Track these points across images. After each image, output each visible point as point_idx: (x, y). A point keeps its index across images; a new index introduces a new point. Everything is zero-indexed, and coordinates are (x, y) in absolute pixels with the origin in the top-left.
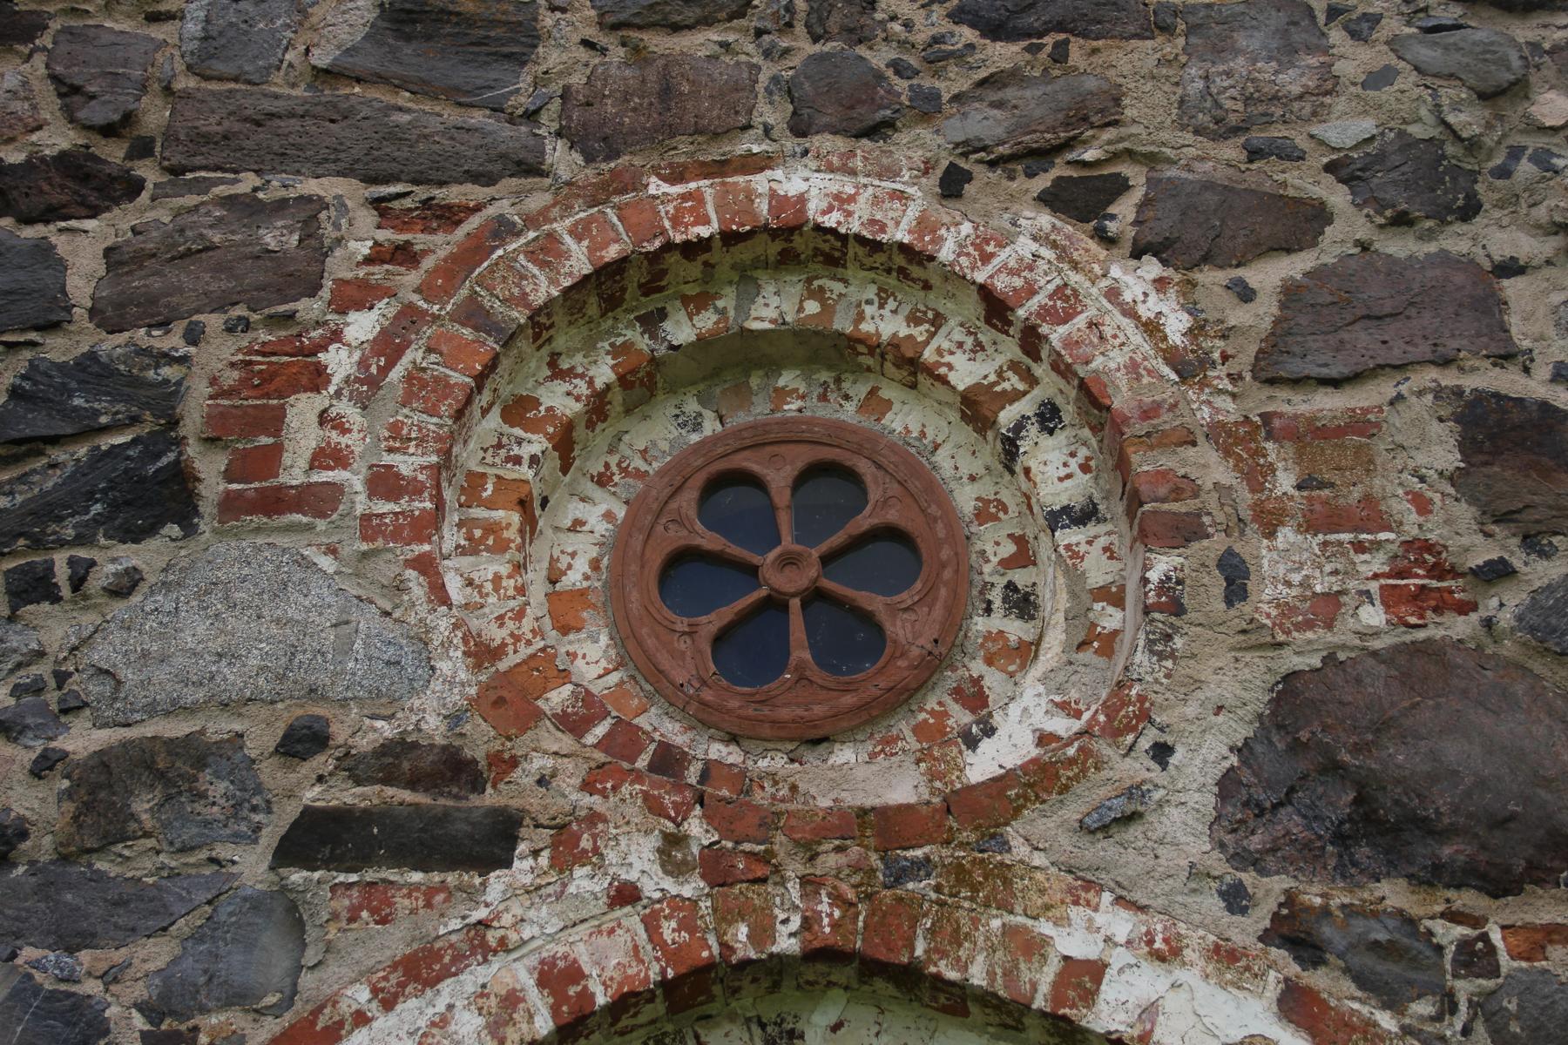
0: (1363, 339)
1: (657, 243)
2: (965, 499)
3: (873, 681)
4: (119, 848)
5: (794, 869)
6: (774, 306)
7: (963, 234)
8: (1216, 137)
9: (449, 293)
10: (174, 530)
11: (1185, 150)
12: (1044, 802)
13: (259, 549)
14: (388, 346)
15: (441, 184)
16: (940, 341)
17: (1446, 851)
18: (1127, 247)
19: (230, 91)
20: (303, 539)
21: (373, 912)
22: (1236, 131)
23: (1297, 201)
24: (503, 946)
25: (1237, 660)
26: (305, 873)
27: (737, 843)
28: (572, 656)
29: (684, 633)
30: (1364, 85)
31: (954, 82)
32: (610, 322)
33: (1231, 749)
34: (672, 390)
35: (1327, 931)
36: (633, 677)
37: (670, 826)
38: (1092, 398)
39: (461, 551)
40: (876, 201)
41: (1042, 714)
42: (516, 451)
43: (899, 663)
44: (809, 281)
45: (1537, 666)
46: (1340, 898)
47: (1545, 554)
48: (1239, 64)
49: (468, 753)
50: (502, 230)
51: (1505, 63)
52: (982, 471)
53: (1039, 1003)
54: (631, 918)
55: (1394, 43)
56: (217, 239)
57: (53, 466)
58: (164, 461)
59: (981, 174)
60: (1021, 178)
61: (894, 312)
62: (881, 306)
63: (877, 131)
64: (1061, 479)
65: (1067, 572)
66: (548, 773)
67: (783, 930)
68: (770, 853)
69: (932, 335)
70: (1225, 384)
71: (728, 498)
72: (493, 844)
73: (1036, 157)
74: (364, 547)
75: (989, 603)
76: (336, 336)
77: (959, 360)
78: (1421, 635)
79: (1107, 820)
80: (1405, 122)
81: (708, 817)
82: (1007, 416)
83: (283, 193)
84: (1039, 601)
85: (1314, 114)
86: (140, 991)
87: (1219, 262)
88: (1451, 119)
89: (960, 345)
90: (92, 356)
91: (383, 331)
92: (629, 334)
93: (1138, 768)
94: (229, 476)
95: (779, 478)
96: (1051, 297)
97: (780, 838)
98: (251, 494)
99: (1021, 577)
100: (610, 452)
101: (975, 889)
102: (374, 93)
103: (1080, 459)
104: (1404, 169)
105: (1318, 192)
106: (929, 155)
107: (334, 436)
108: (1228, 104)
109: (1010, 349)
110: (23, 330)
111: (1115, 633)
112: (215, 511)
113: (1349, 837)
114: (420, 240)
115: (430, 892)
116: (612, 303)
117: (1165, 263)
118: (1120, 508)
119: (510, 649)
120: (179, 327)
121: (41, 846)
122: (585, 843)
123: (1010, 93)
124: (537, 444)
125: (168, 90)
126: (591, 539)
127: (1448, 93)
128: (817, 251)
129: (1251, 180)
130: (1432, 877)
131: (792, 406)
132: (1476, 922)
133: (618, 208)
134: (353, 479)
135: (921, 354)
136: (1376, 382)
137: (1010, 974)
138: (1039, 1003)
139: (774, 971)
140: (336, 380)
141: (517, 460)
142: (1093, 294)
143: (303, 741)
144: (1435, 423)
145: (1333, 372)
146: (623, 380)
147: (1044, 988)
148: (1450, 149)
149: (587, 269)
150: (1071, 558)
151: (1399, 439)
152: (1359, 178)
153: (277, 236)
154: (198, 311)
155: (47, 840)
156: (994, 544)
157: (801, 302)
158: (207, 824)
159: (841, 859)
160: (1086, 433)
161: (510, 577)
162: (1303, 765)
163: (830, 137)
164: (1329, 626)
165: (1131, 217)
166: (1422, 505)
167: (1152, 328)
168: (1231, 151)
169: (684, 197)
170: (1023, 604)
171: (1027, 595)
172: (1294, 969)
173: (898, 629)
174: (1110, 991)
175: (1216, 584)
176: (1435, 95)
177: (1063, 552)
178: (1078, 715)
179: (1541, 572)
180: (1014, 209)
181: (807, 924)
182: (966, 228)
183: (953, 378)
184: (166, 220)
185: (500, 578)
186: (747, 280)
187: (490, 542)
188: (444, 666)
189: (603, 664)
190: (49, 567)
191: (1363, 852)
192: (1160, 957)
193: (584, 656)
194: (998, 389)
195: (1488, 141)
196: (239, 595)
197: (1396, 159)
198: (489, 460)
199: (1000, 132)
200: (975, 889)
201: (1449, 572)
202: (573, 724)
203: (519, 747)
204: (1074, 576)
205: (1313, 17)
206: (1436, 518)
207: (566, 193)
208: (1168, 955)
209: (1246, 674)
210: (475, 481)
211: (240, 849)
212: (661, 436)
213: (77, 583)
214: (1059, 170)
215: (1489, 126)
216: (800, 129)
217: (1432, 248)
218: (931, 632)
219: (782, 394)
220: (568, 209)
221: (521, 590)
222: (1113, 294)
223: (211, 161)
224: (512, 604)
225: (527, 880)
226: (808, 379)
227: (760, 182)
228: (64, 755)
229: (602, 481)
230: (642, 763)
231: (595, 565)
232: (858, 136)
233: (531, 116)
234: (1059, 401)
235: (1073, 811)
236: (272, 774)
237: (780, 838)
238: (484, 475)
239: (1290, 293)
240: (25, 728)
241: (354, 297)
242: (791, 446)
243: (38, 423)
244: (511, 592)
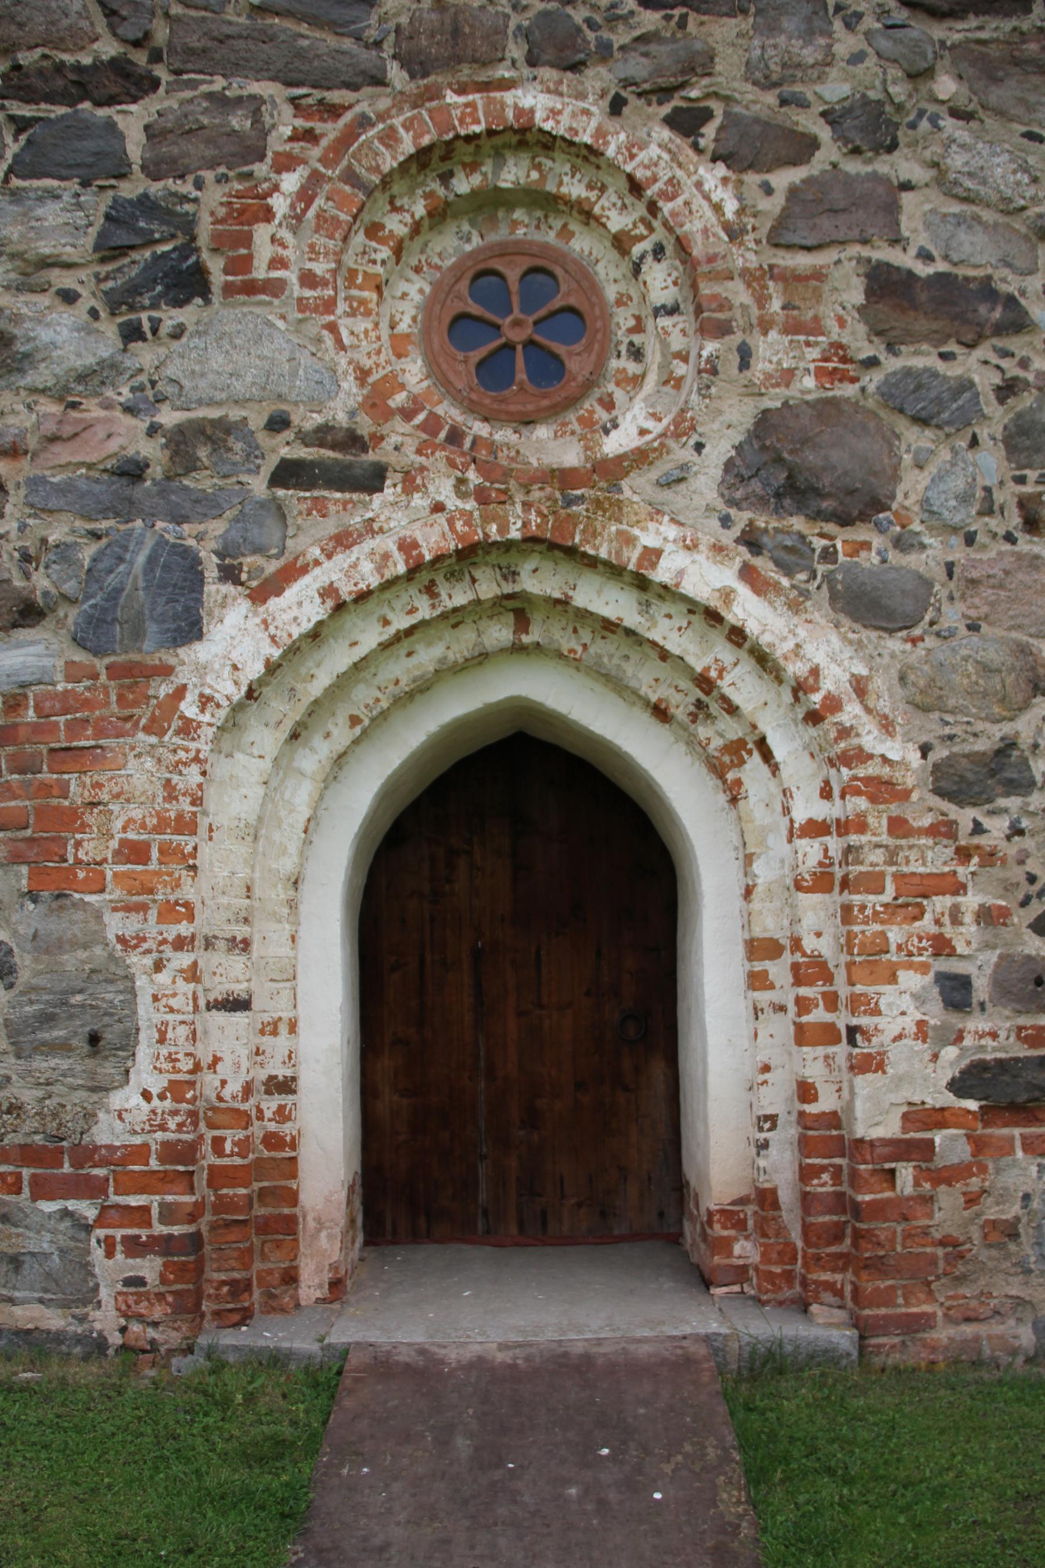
0: (826, 223)
1: (451, 135)
2: (611, 293)
3: (558, 393)
5: (519, 498)
6: (514, 173)
9: (336, 162)
10: (198, 301)
13: (244, 315)
14: (305, 195)
15: (329, 89)
16: (603, 202)
18: (709, 155)
19: (204, 19)
20: (267, 309)
22: (776, 85)
23: (803, 135)
24: (381, 530)
28: (404, 371)
30: (848, 62)
31: (621, 37)
34: (455, 217)
35: (765, 540)
38: (682, 246)
39: (348, 315)
40: (574, 115)
42: (373, 256)
44: (533, 158)
45: (883, 413)
46: (774, 524)
47: (896, 354)
48: (782, 40)
49: (359, 432)
50: (364, 122)
51: (923, 55)
53: (631, 567)
54: (441, 518)
55: (868, 35)
56: (205, 121)
57: (133, 262)
59: (634, 102)
60: (655, 105)
63: (575, 67)
66: (399, 443)
67: (513, 528)
68: (507, 490)
70: (752, 245)
71: (484, 281)
72: (373, 480)
73: (664, 93)
74: (300, 316)
76: (276, 188)
77: (613, 214)
78: (830, 394)
81: (478, 470)
82: (637, 250)
83: (239, 92)
86: (213, 545)
88: (891, 90)
90: (145, 196)
91: (302, 187)
93: (686, 454)
94: (226, 272)
95: (513, 276)
97: (512, 482)
99: (637, 339)
100: (422, 252)
101: (605, 511)
102: (289, 24)
107: (280, 250)
108: (773, 67)
109: (641, 210)
110: (107, 178)
111: (682, 378)
114: (319, 127)
115: (345, 503)
116: (423, 166)
117: (728, 167)
118: (691, 308)
120: (190, 179)
121: (156, 471)
122: (419, 481)
123: (653, 48)
124: (384, 253)
125: (167, 15)
127: (894, 72)
128: (538, 142)
129: (779, 120)
130: (818, 516)
131: (520, 232)
132: (831, 538)
133: (430, 111)
134: (291, 276)
137: (618, 553)
138: (631, 567)
139: (508, 546)
140: (279, 216)
141: (374, 262)
142: (688, 183)
143: (278, 423)
145: (808, 243)
146: (430, 214)
147: (634, 560)
148: (888, 108)
149: (412, 150)
153: (239, 121)
155: (159, 469)
156: (624, 319)
158: (234, 464)
159: (542, 494)
160: (677, 263)
162: (765, 457)
164: (787, 386)
165: (713, 136)
166: (842, 322)
167: (718, 208)
168: (770, 98)
169: (467, 105)
170: (637, 353)
172: (748, 556)
173: (573, 365)
174: (663, 563)
175: (735, 359)
176: (885, 73)
178: (660, 420)
179: (892, 364)
181: (525, 525)
182: (622, 137)
183: (609, 225)
184: (176, 106)
186: (498, 157)
188: (345, 385)
190: (139, 321)
191: (787, 502)
192: (688, 548)
195: (908, 106)
196: (238, 341)
197: (858, 112)
199: (645, 74)
200: (605, 511)
202: (408, 414)
203: (385, 430)
204: (665, 344)
205: (826, 10)
206: (848, 330)
207: (401, 99)
208: (691, 547)
209: (744, 408)
210: (353, 273)
212: (452, 245)
213: (155, 331)
214: (676, 102)
215: (910, 96)
216: (532, 61)
217: (869, 169)
218: (589, 368)
220: (401, 110)
221: (379, 338)
222: (699, 185)
223: (197, 67)
225: (391, 499)
226: (530, 214)
227: (509, 97)
228: (161, 426)
229: (418, 270)
230: (442, 435)
231: (414, 319)
232: (566, 69)
233: (378, 44)
234: (665, 243)
235: (654, 474)
236: (263, 439)
237: (512, 482)
239: (793, 192)
240: (140, 411)
241: (285, 163)
243: (122, 237)
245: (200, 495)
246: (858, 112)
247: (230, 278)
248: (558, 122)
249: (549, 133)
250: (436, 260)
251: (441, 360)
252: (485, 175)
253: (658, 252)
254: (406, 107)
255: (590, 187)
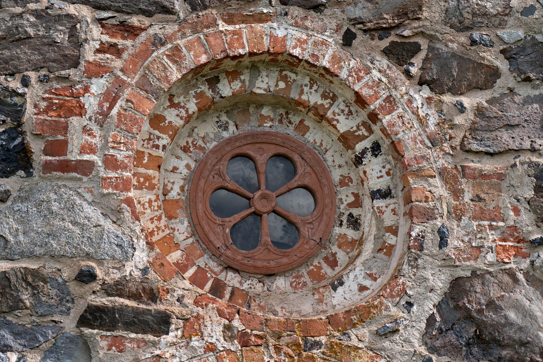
2: (336, 175)
4: (16, 312)
6: (265, 83)
7: (351, 66)
8: (459, 30)
10: (21, 173)
11: (445, 35)
12: (364, 322)
16: (334, 108)
17: (504, 353)
18: (417, 80)
20: (78, 184)
21: (117, 347)
25: (440, 271)
26: (90, 330)
27: (251, 330)
29: (220, 225)
32: (195, 81)
33: (434, 306)
36: (197, 241)
37: (227, 322)
38: (396, 148)
40: (315, 44)
41: (362, 278)
42: (157, 142)
43: (306, 246)
44: (281, 71)
50: (158, 42)
52: (344, 164)
58: (17, 142)
60: (377, 40)
61: (316, 91)
62: (311, 88)
64: (378, 178)
65: (376, 218)
69: (331, 105)
70: (448, 150)
72: (162, 323)
73: (383, 31)
75: (342, 221)
77: (341, 118)
79: (387, 332)
80: (535, 33)
84: (362, 222)
85: (500, 24)
87: (453, 91)
89: (343, 111)
92: (203, 88)
96: (384, 101)
98: (56, 162)
99: (355, 212)
100: (189, 136)
103: (386, 170)
104: (532, 55)
105: (498, 63)
106: (339, 22)
108: (466, 15)
112: (41, 168)
113: (471, 344)
115: (138, 341)
117: (432, 89)
119: (156, 233)
120: (18, 76)
126: (180, 176)
135: (326, 114)
136: (508, 155)
140: (89, 113)
141: (157, 147)
144: (527, 177)
146: (200, 110)
150: (379, 213)
151: (512, 182)
152: (514, 58)
154: (27, 70)
156: (346, 196)
157: (277, 81)
158: (50, 306)
161: (155, 201)
162: (458, 315)
163: (297, 8)
166: (517, 211)
168: (463, 39)
169: (234, 33)
171: (357, 219)
177: (376, 210)
178: (375, 279)
180: (372, 55)
183: (338, 126)
185: (152, 201)
187: (147, 184)
189: (186, 234)
191: (475, 350)
193: (178, 230)
194: (357, 134)
198: (146, 146)
201: (522, 240)
204: (379, 221)
211: (63, 317)
219: (263, 118)
224: (157, 213)
229: (185, 149)
231: (182, 188)
232: (309, 9)
236: (74, 288)
238: (143, 152)
241: (97, 70)
242: (267, 145)
244: (156, 208)
245: (21, 329)
246: (529, 50)
247: (49, 158)
248: (304, 50)
249: (297, 57)
250: (200, 143)
251: (204, 223)
252: (243, 82)
253: (376, 149)
254: (188, 31)
255: (324, 96)
